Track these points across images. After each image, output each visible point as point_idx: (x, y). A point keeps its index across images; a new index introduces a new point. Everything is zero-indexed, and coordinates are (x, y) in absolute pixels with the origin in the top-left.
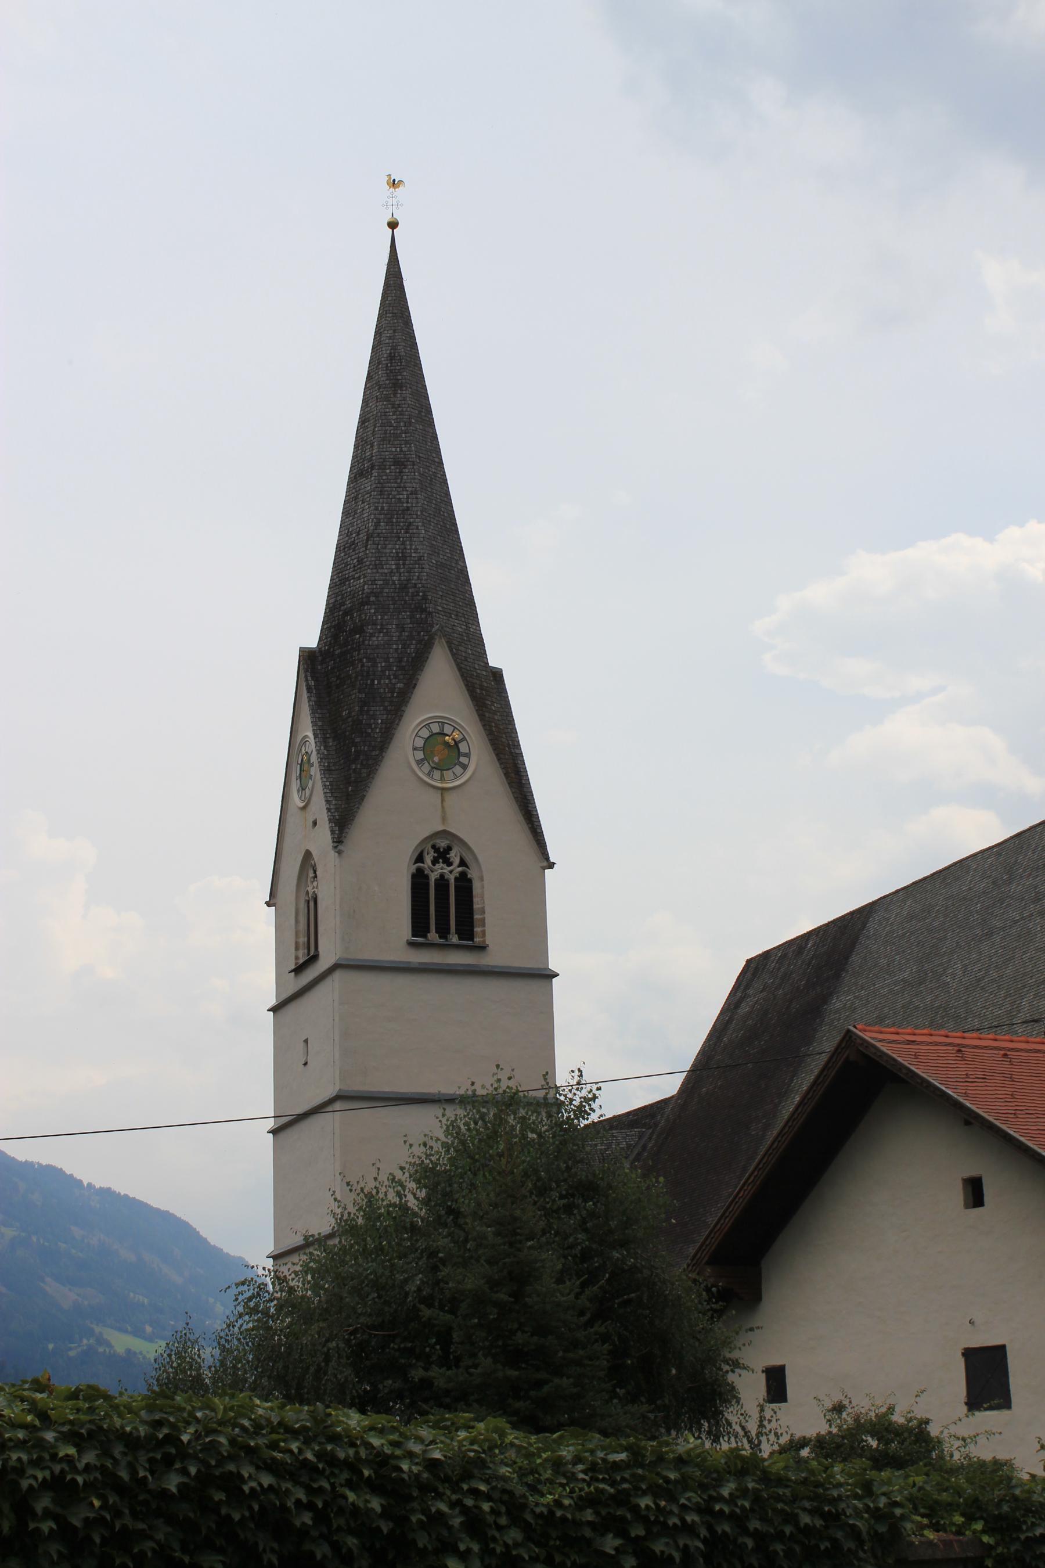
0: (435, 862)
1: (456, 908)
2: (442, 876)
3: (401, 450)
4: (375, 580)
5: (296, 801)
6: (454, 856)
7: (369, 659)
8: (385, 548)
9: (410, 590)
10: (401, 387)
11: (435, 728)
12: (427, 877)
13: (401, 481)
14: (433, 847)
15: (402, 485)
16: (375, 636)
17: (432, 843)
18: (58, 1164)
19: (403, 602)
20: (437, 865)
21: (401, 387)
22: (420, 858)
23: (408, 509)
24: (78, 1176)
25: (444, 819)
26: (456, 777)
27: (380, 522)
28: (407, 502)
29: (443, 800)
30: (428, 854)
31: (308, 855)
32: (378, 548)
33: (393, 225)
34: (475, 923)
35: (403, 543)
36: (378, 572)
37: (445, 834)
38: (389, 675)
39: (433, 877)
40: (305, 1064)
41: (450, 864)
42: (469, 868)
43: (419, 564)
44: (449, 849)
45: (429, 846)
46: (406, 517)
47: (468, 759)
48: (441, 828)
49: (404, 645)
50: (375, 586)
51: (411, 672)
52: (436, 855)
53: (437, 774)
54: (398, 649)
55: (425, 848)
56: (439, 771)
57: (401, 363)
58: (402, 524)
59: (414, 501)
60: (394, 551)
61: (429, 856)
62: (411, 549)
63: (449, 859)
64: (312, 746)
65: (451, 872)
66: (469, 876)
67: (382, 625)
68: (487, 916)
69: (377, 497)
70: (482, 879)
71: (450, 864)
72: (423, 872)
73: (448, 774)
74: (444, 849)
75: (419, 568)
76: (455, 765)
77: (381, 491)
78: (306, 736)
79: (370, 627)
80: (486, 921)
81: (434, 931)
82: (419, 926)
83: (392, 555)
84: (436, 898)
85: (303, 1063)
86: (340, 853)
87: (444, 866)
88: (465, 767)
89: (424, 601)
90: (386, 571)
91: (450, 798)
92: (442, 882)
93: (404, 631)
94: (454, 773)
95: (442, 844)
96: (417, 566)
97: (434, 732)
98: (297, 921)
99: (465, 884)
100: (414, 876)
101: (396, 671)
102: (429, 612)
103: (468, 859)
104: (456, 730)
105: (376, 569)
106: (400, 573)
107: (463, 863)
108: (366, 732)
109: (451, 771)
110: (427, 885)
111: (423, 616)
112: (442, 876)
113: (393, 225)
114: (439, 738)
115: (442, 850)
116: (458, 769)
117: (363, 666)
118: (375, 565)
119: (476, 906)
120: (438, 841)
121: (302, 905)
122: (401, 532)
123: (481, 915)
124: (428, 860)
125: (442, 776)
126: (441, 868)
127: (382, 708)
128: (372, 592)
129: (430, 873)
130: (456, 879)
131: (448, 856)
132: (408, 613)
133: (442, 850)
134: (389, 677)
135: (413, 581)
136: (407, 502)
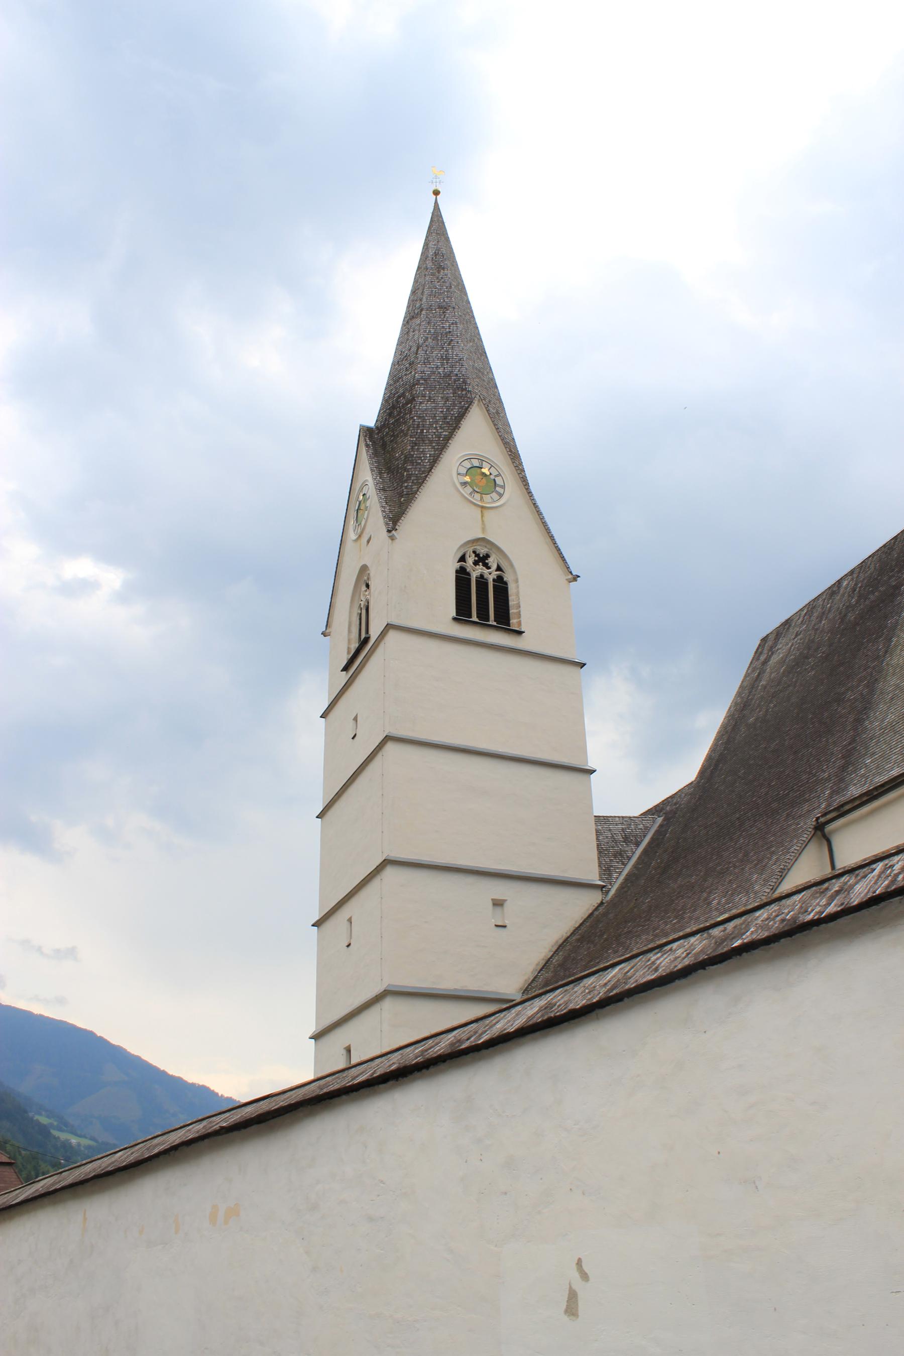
0: (476, 563)
1: (495, 601)
2: (482, 576)
3: (444, 301)
4: (424, 371)
5: (352, 535)
6: (492, 561)
7: (419, 417)
8: (432, 353)
9: (453, 378)
10: (443, 269)
11: (476, 463)
12: (469, 574)
13: (444, 318)
14: (474, 552)
15: (445, 319)
16: (424, 404)
17: (473, 548)
18: (208, 1085)
19: (447, 384)
20: (478, 566)
21: (443, 269)
22: (463, 559)
23: (450, 332)
24: (216, 1091)
25: (484, 529)
26: (494, 502)
27: (427, 339)
28: (450, 329)
29: (482, 516)
30: (469, 557)
31: (364, 569)
32: (426, 353)
33: (436, 193)
34: (511, 616)
35: (447, 351)
36: (426, 367)
37: (483, 540)
38: (436, 427)
39: (474, 575)
40: (348, 946)
41: (489, 568)
42: (503, 572)
43: (459, 363)
44: (487, 556)
45: (471, 550)
46: (448, 336)
47: (503, 490)
48: (481, 536)
49: (448, 410)
50: (424, 375)
51: (454, 425)
52: (476, 558)
53: (477, 496)
54: (443, 411)
55: (467, 551)
56: (480, 494)
57: (443, 257)
58: (445, 340)
59: (455, 328)
60: (439, 355)
61: (471, 558)
62: (453, 354)
63: (488, 564)
64: (371, 490)
65: (491, 576)
66: (505, 579)
67: (430, 397)
68: (522, 609)
69: (425, 325)
70: (517, 581)
71: (489, 568)
72: (466, 570)
73: (487, 498)
74: (483, 555)
75: (459, 365)
76: (493, 492)
77: (428, 322)
78: (366, 481)
79: (420, 398)
80: (521, 613)
81: (476, 617)
82: (462, 613)
83: (438, 357)
84: (477, 590)
85: (347, 945)
86: (392, 538)
87: (484, 568)
88: (501, 495)
89: (464, 384)
90: (433, 366)
91: (487, 514)
92: (482, 583)
93: (448, 401)
94: (491, 498)
95: (482, 551)
96: (458, 364)
97: (475, 465)
98: (349, 631)
99: (502, 587)
100: (457, 572)
101: (441, 424)
102: (468, 390)
103: (504, 566)
104: (492, 468)
105: (425, 364)
106: (444, 368)
107: (499, 568)
108: (416, 462)
109: (489, 495)
110: (469, 580)
111: (464, 393)
112: (482, 576)
113: (436, 193)
114: (479, 470)
115: (481, 556)
116: (494, 495)
117: (414, 421)
118: (424, 362)
119: (512, 603)
120: (478, 547)
121: (356, 611)
122: (444, 345)
123: (517, 609)
124: (470, 560)
125: (482, 498)
126: (480, 569)
127: (430, 447)
128: (422, 378)
129: (472, 571)
130: (494, 580)
131: (487, 561)
132: (451, 391)
133: (481, 556)
134: (436, 428)
135: (455, 373)
136: (450, 329)
